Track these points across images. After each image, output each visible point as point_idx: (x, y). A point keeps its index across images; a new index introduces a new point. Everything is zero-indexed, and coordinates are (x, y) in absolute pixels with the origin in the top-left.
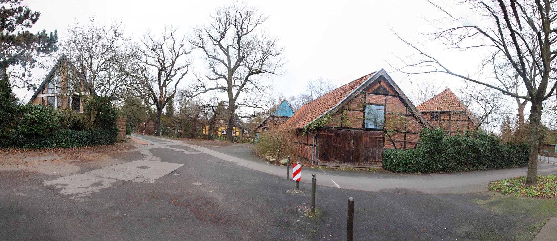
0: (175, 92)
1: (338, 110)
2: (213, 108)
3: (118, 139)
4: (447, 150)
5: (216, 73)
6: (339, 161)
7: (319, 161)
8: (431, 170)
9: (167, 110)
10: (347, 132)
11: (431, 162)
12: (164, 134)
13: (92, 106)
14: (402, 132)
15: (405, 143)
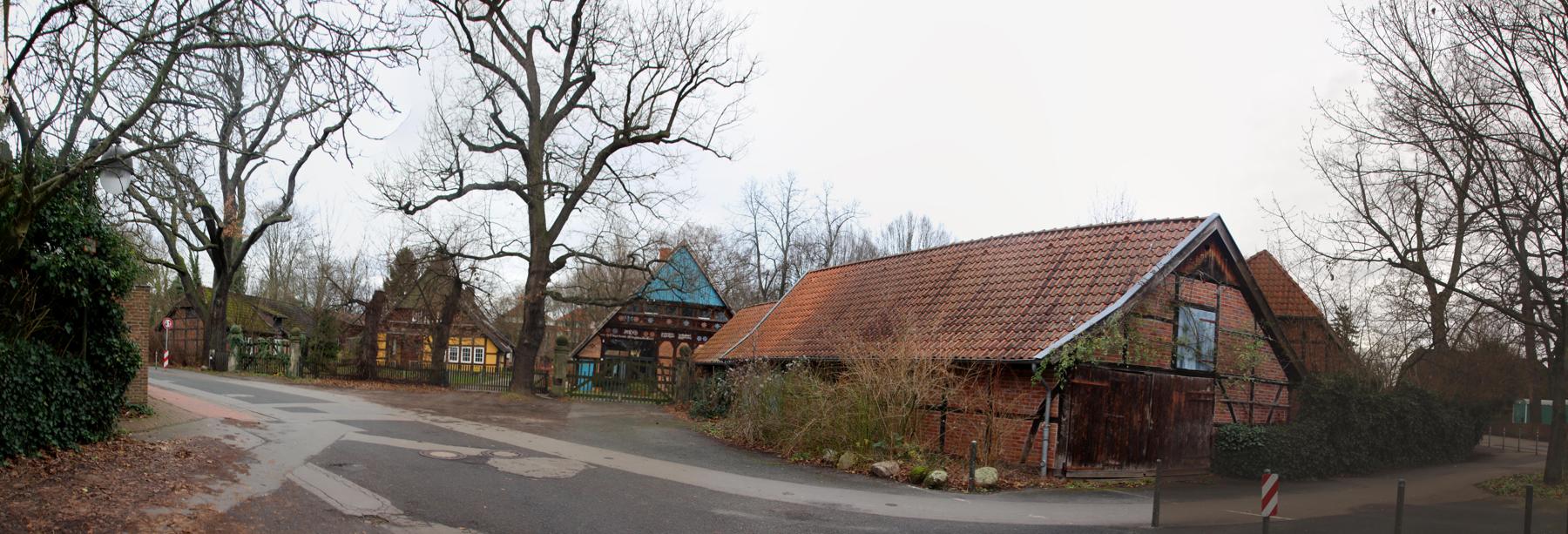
6: (1117, 463)
7: (1069, 464)
10: (1138, 379)
12: (247, 364)
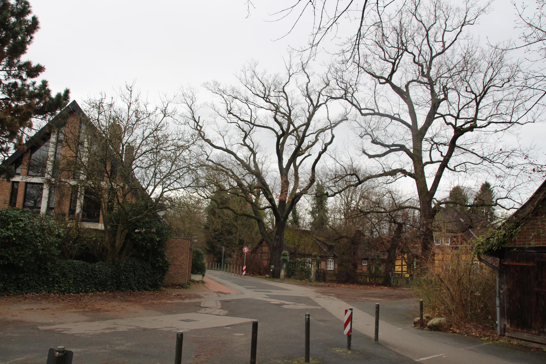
3: (166, 279)
7: (508, 326)
12: (290, 275)
13: (119, 219)
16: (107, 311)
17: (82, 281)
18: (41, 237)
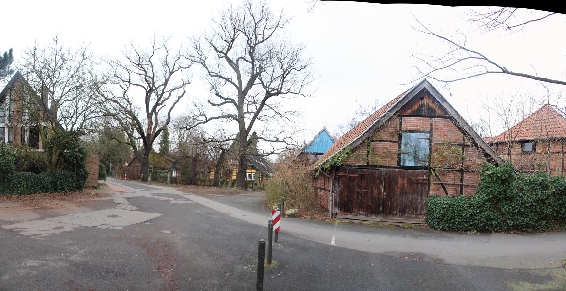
0: (168, 122)
1: (361, 142)
2: (220, 143)
3: (87, 184)
4: (521, 197)
5: (221, 97)
6: (365, 213)
7: (338, 212)
8: (496, 227)
9: (161, 146)
10: (375, 172)
11: (494, 215)
14: (457, 171)
15: (462, 186)
16: (51, 208)
17: (32, 186)
18: (3, 157)
